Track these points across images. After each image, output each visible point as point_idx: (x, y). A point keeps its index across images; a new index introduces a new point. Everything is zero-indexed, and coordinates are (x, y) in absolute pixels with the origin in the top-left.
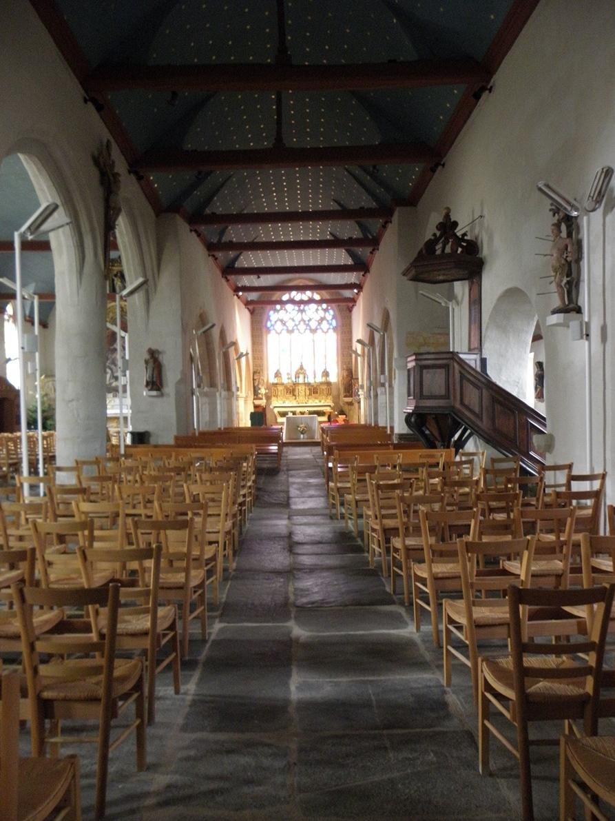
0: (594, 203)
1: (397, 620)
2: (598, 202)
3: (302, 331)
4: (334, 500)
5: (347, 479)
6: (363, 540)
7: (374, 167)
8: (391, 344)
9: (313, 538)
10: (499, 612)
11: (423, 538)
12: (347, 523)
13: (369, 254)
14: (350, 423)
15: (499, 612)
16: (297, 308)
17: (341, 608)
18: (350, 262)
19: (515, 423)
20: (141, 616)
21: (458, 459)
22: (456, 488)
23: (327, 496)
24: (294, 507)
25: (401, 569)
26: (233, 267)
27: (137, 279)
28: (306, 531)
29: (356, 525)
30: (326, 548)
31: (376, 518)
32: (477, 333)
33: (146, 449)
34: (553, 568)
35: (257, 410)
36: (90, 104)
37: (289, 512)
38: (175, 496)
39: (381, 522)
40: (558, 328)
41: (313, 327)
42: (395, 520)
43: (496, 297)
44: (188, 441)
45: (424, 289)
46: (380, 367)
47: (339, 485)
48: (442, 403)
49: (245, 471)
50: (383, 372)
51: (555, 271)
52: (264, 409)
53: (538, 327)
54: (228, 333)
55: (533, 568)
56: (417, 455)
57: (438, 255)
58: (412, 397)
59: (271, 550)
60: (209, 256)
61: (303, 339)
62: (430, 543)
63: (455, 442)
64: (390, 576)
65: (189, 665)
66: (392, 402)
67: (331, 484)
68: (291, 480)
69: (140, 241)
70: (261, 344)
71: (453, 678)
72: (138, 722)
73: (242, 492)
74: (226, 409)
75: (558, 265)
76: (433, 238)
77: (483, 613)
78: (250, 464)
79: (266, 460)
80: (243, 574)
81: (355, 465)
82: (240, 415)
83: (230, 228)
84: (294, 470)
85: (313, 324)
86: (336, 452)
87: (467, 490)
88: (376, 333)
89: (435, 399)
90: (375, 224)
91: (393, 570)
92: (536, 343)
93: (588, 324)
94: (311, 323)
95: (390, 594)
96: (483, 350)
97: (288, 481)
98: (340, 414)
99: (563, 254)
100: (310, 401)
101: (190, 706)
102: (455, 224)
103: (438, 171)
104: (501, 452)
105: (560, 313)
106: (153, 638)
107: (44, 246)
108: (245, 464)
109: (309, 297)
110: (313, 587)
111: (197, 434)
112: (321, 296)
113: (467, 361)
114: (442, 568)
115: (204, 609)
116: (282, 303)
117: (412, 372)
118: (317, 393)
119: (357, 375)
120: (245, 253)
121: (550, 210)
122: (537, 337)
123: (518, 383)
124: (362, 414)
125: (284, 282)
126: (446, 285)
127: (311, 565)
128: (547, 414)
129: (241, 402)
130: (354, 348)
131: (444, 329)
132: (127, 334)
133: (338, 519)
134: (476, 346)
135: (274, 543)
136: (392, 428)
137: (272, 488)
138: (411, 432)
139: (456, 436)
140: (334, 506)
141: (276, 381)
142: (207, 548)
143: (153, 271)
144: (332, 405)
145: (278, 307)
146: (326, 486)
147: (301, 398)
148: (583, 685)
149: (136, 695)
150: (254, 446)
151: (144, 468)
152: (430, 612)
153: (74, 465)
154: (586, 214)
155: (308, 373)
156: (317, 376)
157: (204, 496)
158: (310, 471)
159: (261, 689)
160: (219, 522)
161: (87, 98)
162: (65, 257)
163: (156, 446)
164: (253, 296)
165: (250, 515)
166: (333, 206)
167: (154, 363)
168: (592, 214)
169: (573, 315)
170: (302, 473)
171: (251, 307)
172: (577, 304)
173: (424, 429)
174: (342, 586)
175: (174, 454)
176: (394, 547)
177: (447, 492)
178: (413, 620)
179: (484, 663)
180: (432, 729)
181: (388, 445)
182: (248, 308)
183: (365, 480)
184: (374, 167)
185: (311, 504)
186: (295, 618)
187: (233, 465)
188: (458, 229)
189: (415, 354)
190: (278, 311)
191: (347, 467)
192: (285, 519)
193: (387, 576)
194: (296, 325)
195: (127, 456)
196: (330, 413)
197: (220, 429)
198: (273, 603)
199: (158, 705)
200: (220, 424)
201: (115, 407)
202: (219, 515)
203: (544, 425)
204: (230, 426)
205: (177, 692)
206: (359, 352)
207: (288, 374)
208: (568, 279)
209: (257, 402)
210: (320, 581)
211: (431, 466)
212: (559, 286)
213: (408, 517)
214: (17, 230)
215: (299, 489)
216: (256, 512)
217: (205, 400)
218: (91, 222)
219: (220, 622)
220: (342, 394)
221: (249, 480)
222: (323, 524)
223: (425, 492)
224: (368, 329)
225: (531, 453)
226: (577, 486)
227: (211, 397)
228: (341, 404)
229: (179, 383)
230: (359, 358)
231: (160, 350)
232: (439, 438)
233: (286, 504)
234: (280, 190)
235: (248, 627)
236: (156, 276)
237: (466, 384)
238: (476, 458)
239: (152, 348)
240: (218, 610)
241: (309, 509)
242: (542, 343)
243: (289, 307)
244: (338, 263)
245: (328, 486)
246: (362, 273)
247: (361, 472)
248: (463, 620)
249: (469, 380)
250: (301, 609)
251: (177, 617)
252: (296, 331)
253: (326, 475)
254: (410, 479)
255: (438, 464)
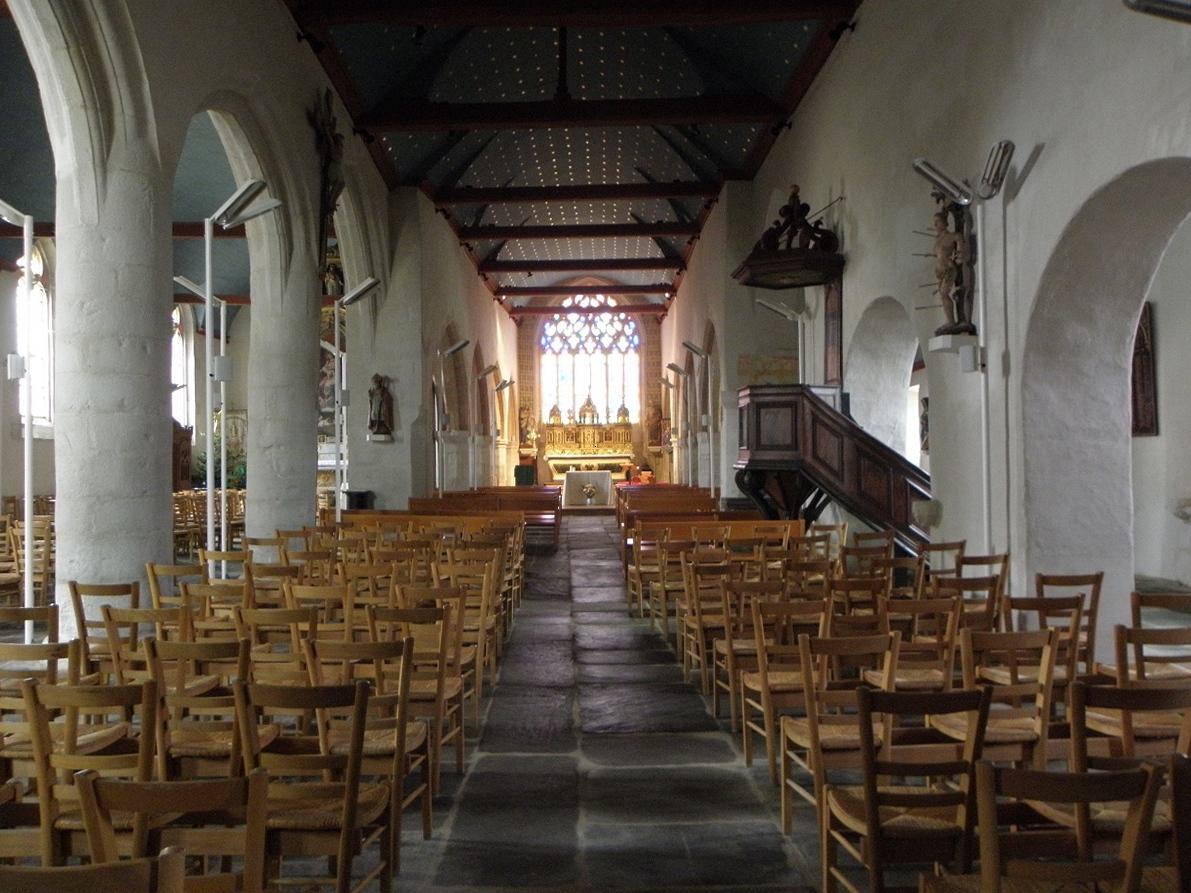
0: (990, 188)
1: (720, 751)
2: (996, 185)
3: (590, 350)
4: (634, 589)
5: (654, 561)
6: (675, 645)
7: (694, 127)
8: (717, 371)
9: (606, 642)
10: (846, 733)
11: (757, 641)
12: (653, 623)
13: (686, 244)
14: (659, 483)
15: (846, 733)
16: (583, 319)
17: (645, 734)
18: (659, 254)
19: (889, 483)
20: (383, 732)
21: (809, 534)
22: (804, 573)
23: (625, 586)
24: (578, 600)
25: (727, 683)
26: (494, 259)
27: (360, 281)
28: (596, 632)
29: (666, 625)
30: (625, 656)
31: (694, 614)
32: (836, 359)
33: (371, 516)
34: (931, 679)
35: (525, 462)
36: (305, 42)
37: (572, 607)
38: (417, 581)
39: (700, 619)
40: (946, 354)
41: (606, 345)
42: (721, 617)
43: (863, 308)
44: (427, 504)
45: (763, 296)
46: (701, 403)
47: (642, 569)
48: (787, 455)
49: (511, 549)
50: (705, 410)
51: (940, 276)
52: (535, 461)
53: (919, 350)
54: (485, 353)
55: (898, 680)
56: (751, 529)
57: (782, 251)
58: (745, 448)
59: (547, 657)
60: (461, 245)
61: (591, 363)
62: (765, 644)
63: (807, 510)
64: (712, 694)
65: (443, 804)
66: (717, 454)
67: (631, 568)
68: (574, 562)
69: (366, 225)
70: (532, 368)
71: (793, 823)
72: (382, 866)
73: (508, 577)
74: (481, 461)
75: (944, 268)
76: (775, 227)
77: (831, 734)
78: (517, 539)
79: (538, 534)
80: (507, 689)
81: (665, 541)
82: (501, 470)
83: (491, 206)
84: (577, 549)
85: (607, 341)
86: (638, 522)
87: (821, 577)
88: (695, 355)
89: (779, 449)
90: (695, 204)
91: (717, 684)
92: (916, 372)
93: (984, 351)
94: (603, 340)
95: (712, 718)
96: (845, 383)
97: (569, 564)
98: (644, 470)
99: (951, 254)
100: (601, 451)
101: (444, 854)
102: (806, 208)
103: (781, 135)
104: (871, 527)
105: (948, 333)
106: (400, 760)
107: (239, 231)
108: (511, 539)
109: (600, 302)
110: (606, 707)
111: (440, 496)
112: (617, 301)
113: (822, 398)
114: (782, 678)
115: (461, 731)
116: (563, 311)
117: (746, 412)
118: (611, 439)
119: (669, 414)
120: (511, 241)
121: (933, 195)
122: (919, 365)
123: (894, 428)
124: (674, 469)
125: (564, 281)
126: (795, 290)
127: (603, 678)
128: (932, 471)
129: (502, 452)
130: (664, 377)
131: (789, 352)
132: (345, 354)
133: (640, 617)
134: (835, 376)
135: (552, 649)
136: (718, 490)
137: (548, 573)
138: (743, 496)
139: (808, 501)
140: (634, 599)
141: (552, 421)
142: (464, 650)
143: (383, 265)
144: (632, 456)
145: (557, 316)
146: (624, 571)
147: (588, 446)
148: (952, 817)
149: (381, 829)
150: (522, 513)
151: (371, 543)
152: (764, 737)
153: (274, 536)
154: (980, 203)
155: (598, 411)
156: (610, 415)
157: (456, 580)
158: (601, 550)
159: (537, 834)
160: (478, 616)
161: (302, 34)
162: (265, 249)
163: (384, 512)
164: (521, 301)
165: (518, 610)
166: (636, 178)
167: (382, 396)
168: (987, 202)
169: (965, 337)
170: (590, 553)
171: (517, 316)
172: (970, 321)
173: (762, 491)
174: (646, 706)
175: (411, 523)
176: (717, 653)
177: (792, 579)
178: (741, 750)
179: (830, 793)
180: (763, 885)
181: (712, 514)
182: (514, 318)
183: (679, 563)
184: (694, 127)
185: (601, 596)
186: (583, 746)
187: (497, 539)
188: (810, 214)
189: (751, 387)
190: (556, 323)
191: (654, 545)
192: (566, 616)
193: (708, 692)
194: (581, 343)
195: (344, 525)
196: (630, 467)
197: (472, 489)
198: (552, 728)
199: (404, 852)
200: (473, 482)
201: (328, 457)
202: (478, 608)
203: (928, 487)
204: (486, 485)
205: (427, 836)
206: (672, 381)
207: (569, 412)
208: (958, 288)
209: (525, 451)
210: (616, 699)
211: (771, 544)
212: (946, 297)
213: (738, 612)
214: (208, 217)
215: (586, 575)
216: (525, 607)
217: (453, 448)
218: (302, 199)
219: (482, 750)
220: (647, 441)
221: (516, 561)
222: (620, 623)
223: (762, 579)
224: (685, 350)
225: (913, 528)
226: (969, 572)
227: (460, 443)
228: (645, 455)
229: (416, 423)
230: (671, 390)
231: (390, 375)
232: (784, 506)
233: (568, 596)
234: (561, 154)
235: (517, 757)
236: (388, 274)
237: (821, 430)
238: (834, 534)
239: (380, 374)
240: (476, 737)
241: (599, 603)
242: (923, 371)
243: (573, 317)
244: (643, 256)
245: (627, 570)
246: (676, 271)
247: (674, 551)
248: (805, 742)
249: (826, 426)
250: (591, 735)
251: (429, 737)
252: (582, 351)
253: (623, 555)
254: (740, 562)
255: (781, 540)
